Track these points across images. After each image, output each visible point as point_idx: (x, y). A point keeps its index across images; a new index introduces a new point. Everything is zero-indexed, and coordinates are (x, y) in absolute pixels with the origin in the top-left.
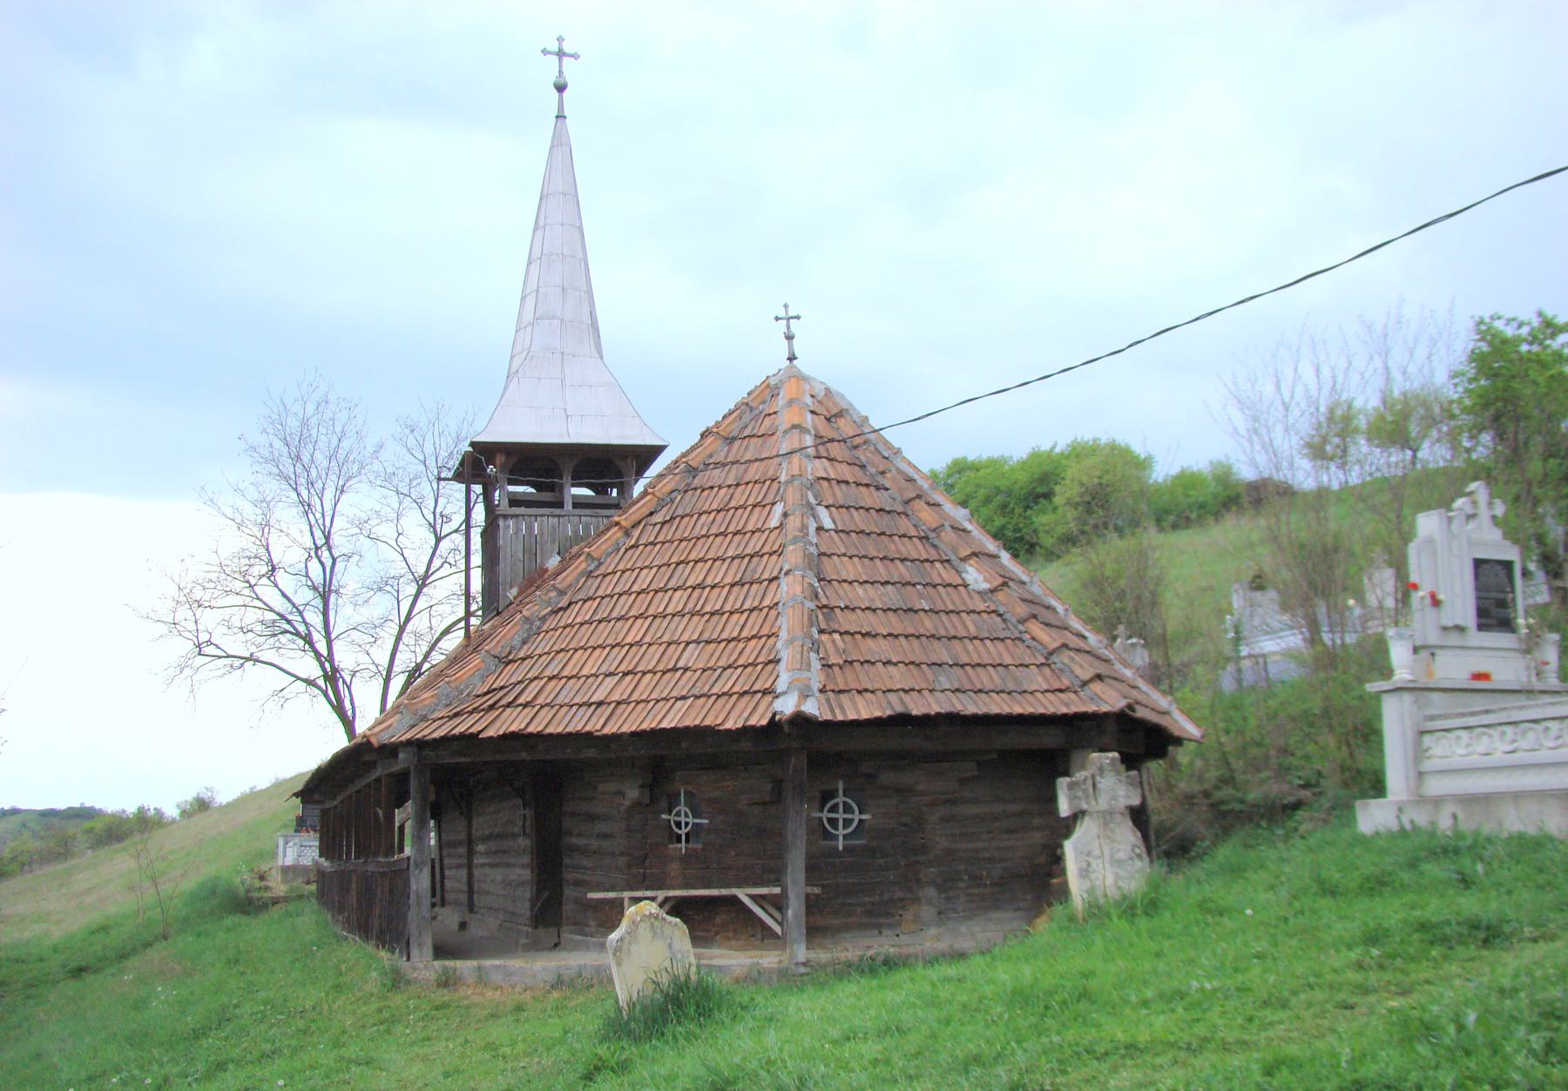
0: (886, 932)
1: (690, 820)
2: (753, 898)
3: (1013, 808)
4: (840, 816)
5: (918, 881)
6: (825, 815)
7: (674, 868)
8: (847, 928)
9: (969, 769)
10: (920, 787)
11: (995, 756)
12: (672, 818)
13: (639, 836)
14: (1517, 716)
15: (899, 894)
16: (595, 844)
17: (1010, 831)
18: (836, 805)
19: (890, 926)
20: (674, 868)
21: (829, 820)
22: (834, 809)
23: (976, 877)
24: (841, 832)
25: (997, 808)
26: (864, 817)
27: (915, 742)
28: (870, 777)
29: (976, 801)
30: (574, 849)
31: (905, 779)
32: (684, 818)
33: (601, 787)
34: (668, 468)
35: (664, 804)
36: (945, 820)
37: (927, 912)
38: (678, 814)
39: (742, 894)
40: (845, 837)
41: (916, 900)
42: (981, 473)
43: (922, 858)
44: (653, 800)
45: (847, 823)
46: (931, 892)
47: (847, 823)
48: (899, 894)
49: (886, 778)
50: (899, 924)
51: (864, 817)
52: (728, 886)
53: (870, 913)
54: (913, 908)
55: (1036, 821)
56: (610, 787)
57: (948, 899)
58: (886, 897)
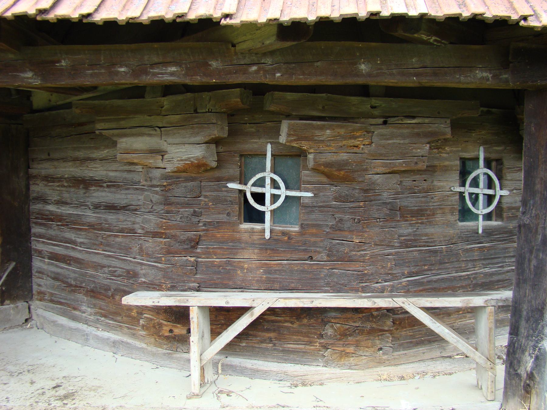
1: (283, 192)
2: (428, 310)
6: (468, 189)
7: (249, 258)
12: (249, 189)
13: (187, 211)
14: (275, 119)
16: (91, 216)
20: (249, 258)
21: (254, 195)
30: (48, 219)
32: (270, 185)
33: (124, 143)
35: (234, 170)
38: (261, 183)
39: (414, 306)
44: (221, 162)
47: (275, 198)
52: (393, 292)
56: (140, 143)
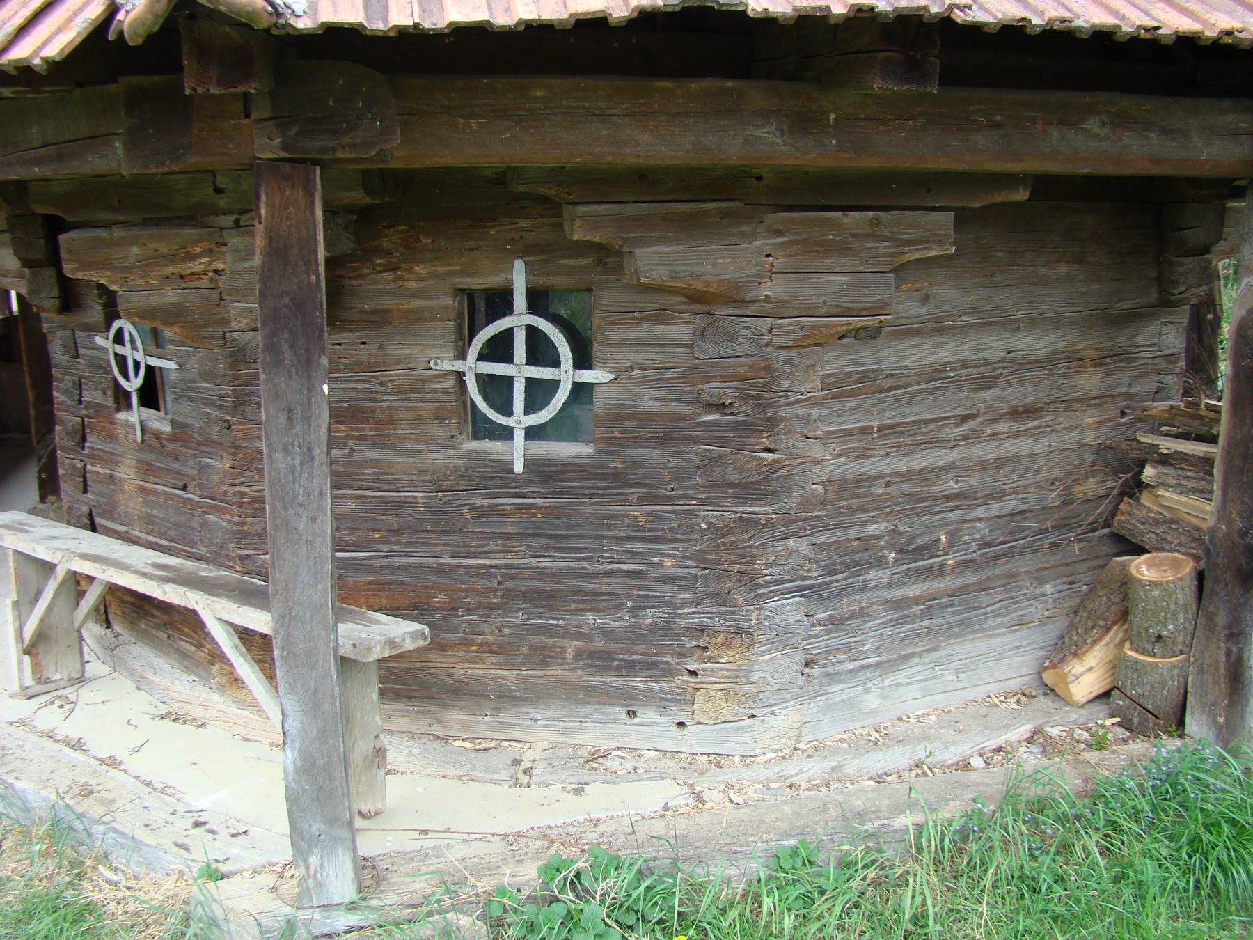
0: (646, 715)
3: (1032, 344)
4: (519, 371)
5: (749, 578)
8: (533, 695)
9: (934, 229)
10: (767, 289)
11: (1021, 195)
15: (691, 614)
17: (1018, 413)
18: (506, 338)
19: (661, 702)
22: (499, 349)
23: (921, 551)
24: (520, 420)
25: (992, 346)
26: (586, 376)
27: (758, 138)
28: (607, 258)
29: (938, 328)
31: (723, 260)
34: (923, 471)
36: (840, 389)
37: (772, 666)
40: (533, 433)
41: (741, 635)
42: (602, 828)
43: (762, 510)
45: (538, 393)
46: (786, 610)
47: (538, 393)
48: (691, 614)
49: (655, 260)
50: (684, 698)
51: (586, 376)
53: (601, 660)
54: (726, 661)
55: (1089, 381)
57: (835, 623)
58: (649, 618)
